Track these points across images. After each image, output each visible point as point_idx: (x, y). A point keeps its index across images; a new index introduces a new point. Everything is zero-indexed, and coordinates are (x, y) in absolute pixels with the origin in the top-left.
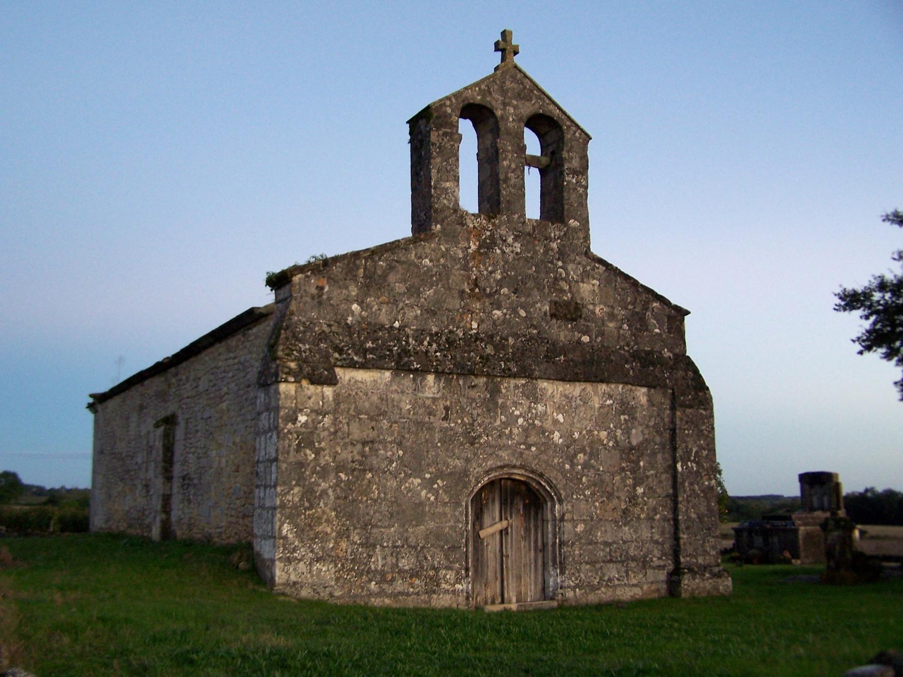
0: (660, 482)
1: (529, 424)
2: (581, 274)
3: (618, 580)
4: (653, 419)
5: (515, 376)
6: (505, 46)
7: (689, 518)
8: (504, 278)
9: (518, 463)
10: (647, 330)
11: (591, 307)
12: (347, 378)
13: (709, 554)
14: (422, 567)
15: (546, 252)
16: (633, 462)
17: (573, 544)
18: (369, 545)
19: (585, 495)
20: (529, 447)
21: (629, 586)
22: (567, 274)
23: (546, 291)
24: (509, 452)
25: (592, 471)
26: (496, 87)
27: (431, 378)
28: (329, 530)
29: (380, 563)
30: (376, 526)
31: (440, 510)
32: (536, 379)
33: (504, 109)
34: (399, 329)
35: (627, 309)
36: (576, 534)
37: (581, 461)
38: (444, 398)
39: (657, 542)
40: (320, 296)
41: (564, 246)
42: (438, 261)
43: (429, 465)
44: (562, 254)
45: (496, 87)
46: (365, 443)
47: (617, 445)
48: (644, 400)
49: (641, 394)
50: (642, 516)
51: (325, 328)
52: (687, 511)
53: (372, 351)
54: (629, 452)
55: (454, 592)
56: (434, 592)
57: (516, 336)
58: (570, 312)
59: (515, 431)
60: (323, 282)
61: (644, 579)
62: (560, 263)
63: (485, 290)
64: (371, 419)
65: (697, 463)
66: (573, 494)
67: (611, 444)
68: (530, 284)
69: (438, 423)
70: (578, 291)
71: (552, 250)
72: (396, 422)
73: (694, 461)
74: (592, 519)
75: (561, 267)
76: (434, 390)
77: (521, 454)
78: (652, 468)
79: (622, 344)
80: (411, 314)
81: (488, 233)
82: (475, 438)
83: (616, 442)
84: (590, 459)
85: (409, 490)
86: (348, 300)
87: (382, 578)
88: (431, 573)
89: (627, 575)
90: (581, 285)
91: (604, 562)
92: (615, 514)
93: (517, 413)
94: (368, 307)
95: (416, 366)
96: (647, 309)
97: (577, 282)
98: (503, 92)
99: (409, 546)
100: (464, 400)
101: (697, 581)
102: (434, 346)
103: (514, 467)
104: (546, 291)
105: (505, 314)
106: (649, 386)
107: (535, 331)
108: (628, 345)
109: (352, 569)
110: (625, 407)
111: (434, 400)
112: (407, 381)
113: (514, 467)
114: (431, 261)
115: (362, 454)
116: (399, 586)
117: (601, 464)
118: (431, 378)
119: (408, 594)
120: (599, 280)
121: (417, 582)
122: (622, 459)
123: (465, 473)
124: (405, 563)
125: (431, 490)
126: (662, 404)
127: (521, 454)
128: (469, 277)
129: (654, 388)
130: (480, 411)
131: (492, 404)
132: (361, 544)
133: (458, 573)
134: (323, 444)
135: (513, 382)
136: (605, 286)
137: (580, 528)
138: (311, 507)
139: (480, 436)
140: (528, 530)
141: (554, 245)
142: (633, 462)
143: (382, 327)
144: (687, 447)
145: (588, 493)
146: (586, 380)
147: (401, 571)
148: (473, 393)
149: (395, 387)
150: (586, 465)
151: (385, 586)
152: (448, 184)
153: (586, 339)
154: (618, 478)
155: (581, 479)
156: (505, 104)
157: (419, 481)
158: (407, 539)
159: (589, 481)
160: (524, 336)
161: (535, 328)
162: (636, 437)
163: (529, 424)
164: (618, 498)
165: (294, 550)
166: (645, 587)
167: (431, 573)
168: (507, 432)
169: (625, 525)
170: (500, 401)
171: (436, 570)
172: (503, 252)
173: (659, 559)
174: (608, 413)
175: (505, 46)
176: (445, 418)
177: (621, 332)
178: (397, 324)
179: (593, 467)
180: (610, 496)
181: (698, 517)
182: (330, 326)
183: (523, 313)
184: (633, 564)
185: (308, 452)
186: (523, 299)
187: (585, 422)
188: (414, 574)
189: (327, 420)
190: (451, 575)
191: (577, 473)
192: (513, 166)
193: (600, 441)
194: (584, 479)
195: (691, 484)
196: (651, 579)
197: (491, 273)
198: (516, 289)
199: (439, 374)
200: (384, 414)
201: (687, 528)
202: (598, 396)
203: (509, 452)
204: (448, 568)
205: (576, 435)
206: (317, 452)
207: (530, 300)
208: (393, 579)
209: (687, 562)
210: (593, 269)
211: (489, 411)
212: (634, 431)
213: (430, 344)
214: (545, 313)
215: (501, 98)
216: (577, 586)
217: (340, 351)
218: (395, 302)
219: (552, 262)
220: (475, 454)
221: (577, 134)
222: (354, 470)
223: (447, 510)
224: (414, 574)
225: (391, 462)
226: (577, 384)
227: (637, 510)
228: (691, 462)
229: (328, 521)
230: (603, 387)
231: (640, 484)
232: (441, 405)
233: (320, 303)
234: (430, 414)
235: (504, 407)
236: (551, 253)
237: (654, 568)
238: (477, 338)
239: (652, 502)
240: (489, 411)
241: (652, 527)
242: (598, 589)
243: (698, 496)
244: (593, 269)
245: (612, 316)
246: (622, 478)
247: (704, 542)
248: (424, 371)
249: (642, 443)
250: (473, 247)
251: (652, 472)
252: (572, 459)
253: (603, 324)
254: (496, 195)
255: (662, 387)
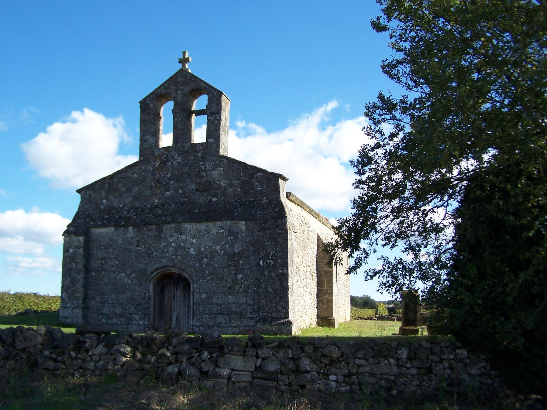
0: (253, 272)
1: (178, 245)
2: (213, 166)
3: (225, 323)
4: (248, 238)
5: (169, 223)
6: (184, 61)
7: (267, 291)
8: (172, 176)
9: (171, 265)
10: (253, 189)
11: (218, 182)
12: (97, 232)
13: (280, 312)
14: (125, 313)
15: (195, 159)
16: (235, 261)
17: (199, 304)
18: (103, 302)
19: (207, 280)
20: (177, 257)
21: (231, 327)
22: (205, 168)
23: (194, 178)
24: (167, 259)
25: (211, 267)
26: (172, 83)
27: (131, 228)
28: (80, 296)
29: (107, 310)
30: (105, 295)
31: (133, 287)
32: (181, 223)
33: (176, 93)
34: (122, 208)
35: (240, 179)
36: (201, 299)
37: (205, 262)
38: (137, 236)
39: (249, 304)
40: (90, 199)
41: (204, 153)
42: (141, 174)
43: (128, 267)
44: (203, 158)
45: (172, 83)
46: (103, 259)
47: (226, 253)
48: (243, 228)
49: (242, 225)
50: (240, 290)
51: (91, 212)
52: (266, 287)
53: (106, 219)
54: (233, 257)
55: (138, 324)
56: (130, 324)
57: (175, 203)
58: (207, 187)
59: (170, 249)
60: (92, 193)
61: (241, 324)
62: (202, 163)
63: (162, 183)
64: (106, 248)
65: (274, 260)
66: (200, 279)
67: (222, 253)
68: (185, 176)
69: (134, 248)
70: (211, 175)
71: (198, 157)
72: (115, 249)
73: (272, 259)
74: (210, 292)
75: (202, 165)
76: (132, 233)
77: (173, 260)
78: (247, 264)
79: (236, 199)
80: (127, 200)
81: (165, 156)
82: (150, 254)
83: (226, 251)
84: (210, 261)
85: (120, 278)
86: (102, 199)
87: (108, 316)
88: (129, 316)
89: (230, 321)
90: (213, 171)
91: (216, 314)
92: (224, 290)
93: (171, 240)
94: (110, 200)
95: (123, 223)
96: (252, 178)
97: (211, 170)
98: (176, 84)
99: (119, 303)
100: (146, 237)
101: (266, 326)
102: (134, 213)
103: (170, 267)
104: (194, 178)
105: (171, 193)
106: (246, 221)
107: (186, 199)
108: (240, 199)
109: (96, 313)
110: (231, 232)
111: (132, 238)
112: (121, 231)
113: (170, 267)
114: (137, 174)
115: (102, 264)
116: (115, 321)
117: (216, 263)
118: (131, 228)
119: (118, 325)
120: (223, 167)
121: (122, 319)
122: (229, 260)
123: (145, 270)
124: (118, 311)
125: (129, 278)
126: (254, 229)
127: (173, 260)
128: (155, 179)
129: (249, 220)
130: (153, 241)
131: (159, 237)
132: (100, 302)
133: (140, 316)
134: (79, 261)
135: (169, 226)
136: (227, 170)
137: (204, 296)
138: (73, 287)
139: (153, 253)
140: (185, 297)
141: (199, 154)
142: (235, 261)
143: (115, 208)
144: (266, 252)
145: (208, 278)
146: (207, 221)
147: (115, 314)
148: (150, 233)
149: (115, 234)
150: (208, 264)
151: (109, 320)
152: (147, 137)
153: (215, 199)
154: (226, 270)
155: (205, 271)
156: (176, 90)
157: (124, 274)
158: (119, 300)
159: (209, 272)
160: (180, 202)
161: (187, 197)
162: (237, 248)
163: (178, 245)
164: (226, 281)
165: (67, 304)
166: (241, 328)
167: (129, 316)
168: (166, 250)
169: (230, 295)
170: (163, 236)
171: (131, 314)
172: (172, 163)
173: (250, 313)
174: (221, 236)
175: (184, 61)
176: (137, 246)
177: (236, 192)
178: (121, 206)
179: (212, 265)
180: (221, 280)
181: (274, 291)
182: (93, 211)
183: (181, 191)
184: (234, 316)
185: (73, 264)
186: (181, 185)
187: (207, 242)
188: (121, 316)
189: (81, 251)
190: (137, 317)
191: (203, 268)
192: (180, 120)
193: (217, 252)
194: (207, 271)
195: (269, 272)
196: (245, 324)
197: (165, 174)
198: (178, 180)
199: (134, 226)
200: (110, 246)
201: (266, 297)
202: (216, 228)
203: (167, 259)
204: (136, 314)
205: (203, 249)
206: (76, 264)
207: (185, 184)
208: (112, 318)
209: (265, 315)
210: (220, 162)
211: (157, 241)
212: (236, 245)
213: (133, 213)
214: (193, 189)
215: (175, 88)
216: (201, 325)
217: (94, 220)
218: (121, 197)
219: (197, 163)
220: (150, 261)
221: (215, 93)
222: (98, 271)
223: (136, 287)
224: (121, 316)
225: (113, 266)
226: (204, 223)
227: (237, 287)
228: (269, 260)
229: (80, 292)
230: (219, 223)
231: (240, 273)
232: (135, 239)
233: (90, 202)
234: (130, 244)
235: (165, 238)
236: (197, 159)
237: (247, 318)
238: (157, 207)
239: (247, 283)
240: (157, 241)
241: (247, 296)
242: (213, 328)
243: (274, 279)
244: (220, 162)
245: (231, 185)
246: (229, 270)
247: (277, 305)
248: (126, 226)
249: (241, 251)
250: (157, 164)
251: (247, 266)
252: (200, 261)
253: (225, 190)
254: (182, 131)
255: (253, 220)
